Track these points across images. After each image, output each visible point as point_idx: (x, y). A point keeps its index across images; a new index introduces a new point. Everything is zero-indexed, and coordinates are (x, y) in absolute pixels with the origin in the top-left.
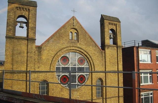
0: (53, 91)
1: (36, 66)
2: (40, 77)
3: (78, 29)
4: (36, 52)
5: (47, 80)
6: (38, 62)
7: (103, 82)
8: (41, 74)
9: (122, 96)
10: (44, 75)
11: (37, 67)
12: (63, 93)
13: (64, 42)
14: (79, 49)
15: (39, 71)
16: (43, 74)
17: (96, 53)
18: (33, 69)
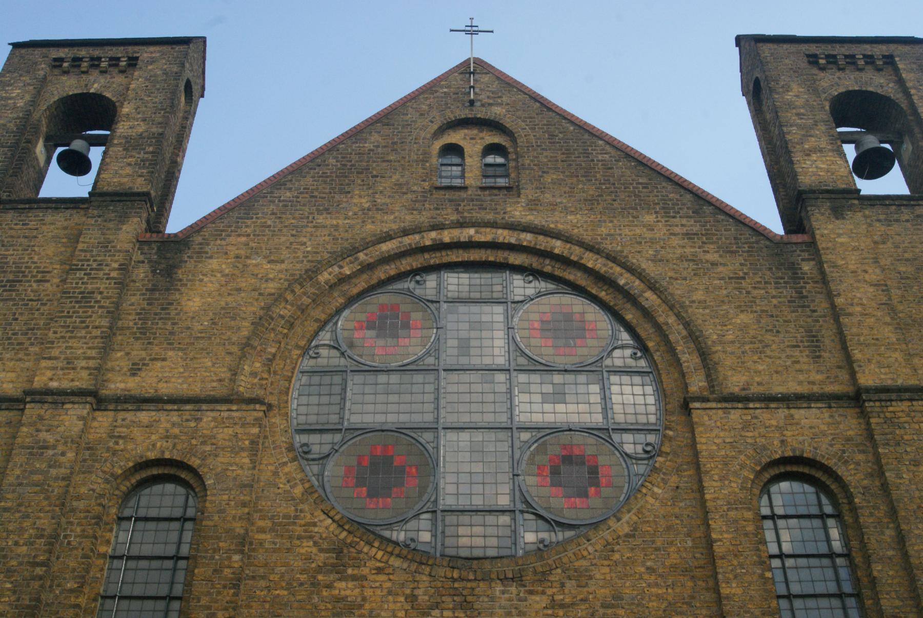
0: (236, 557)
1: (119, 360)
2: (137, 432)
3: (508, 122)
4: (141, 273)
5: (195, 462)
6: (144, 334)
7: (850, 497)
8: (144, 416)
9: (802, 591)
10: (175, 419)
11: (125, 365)
12: (346, 589)
13: (380, 200)
14: (527, 238)
15: (136, 392)
16: (167, 420)
17: (713, 257)
18: (84, 374)
